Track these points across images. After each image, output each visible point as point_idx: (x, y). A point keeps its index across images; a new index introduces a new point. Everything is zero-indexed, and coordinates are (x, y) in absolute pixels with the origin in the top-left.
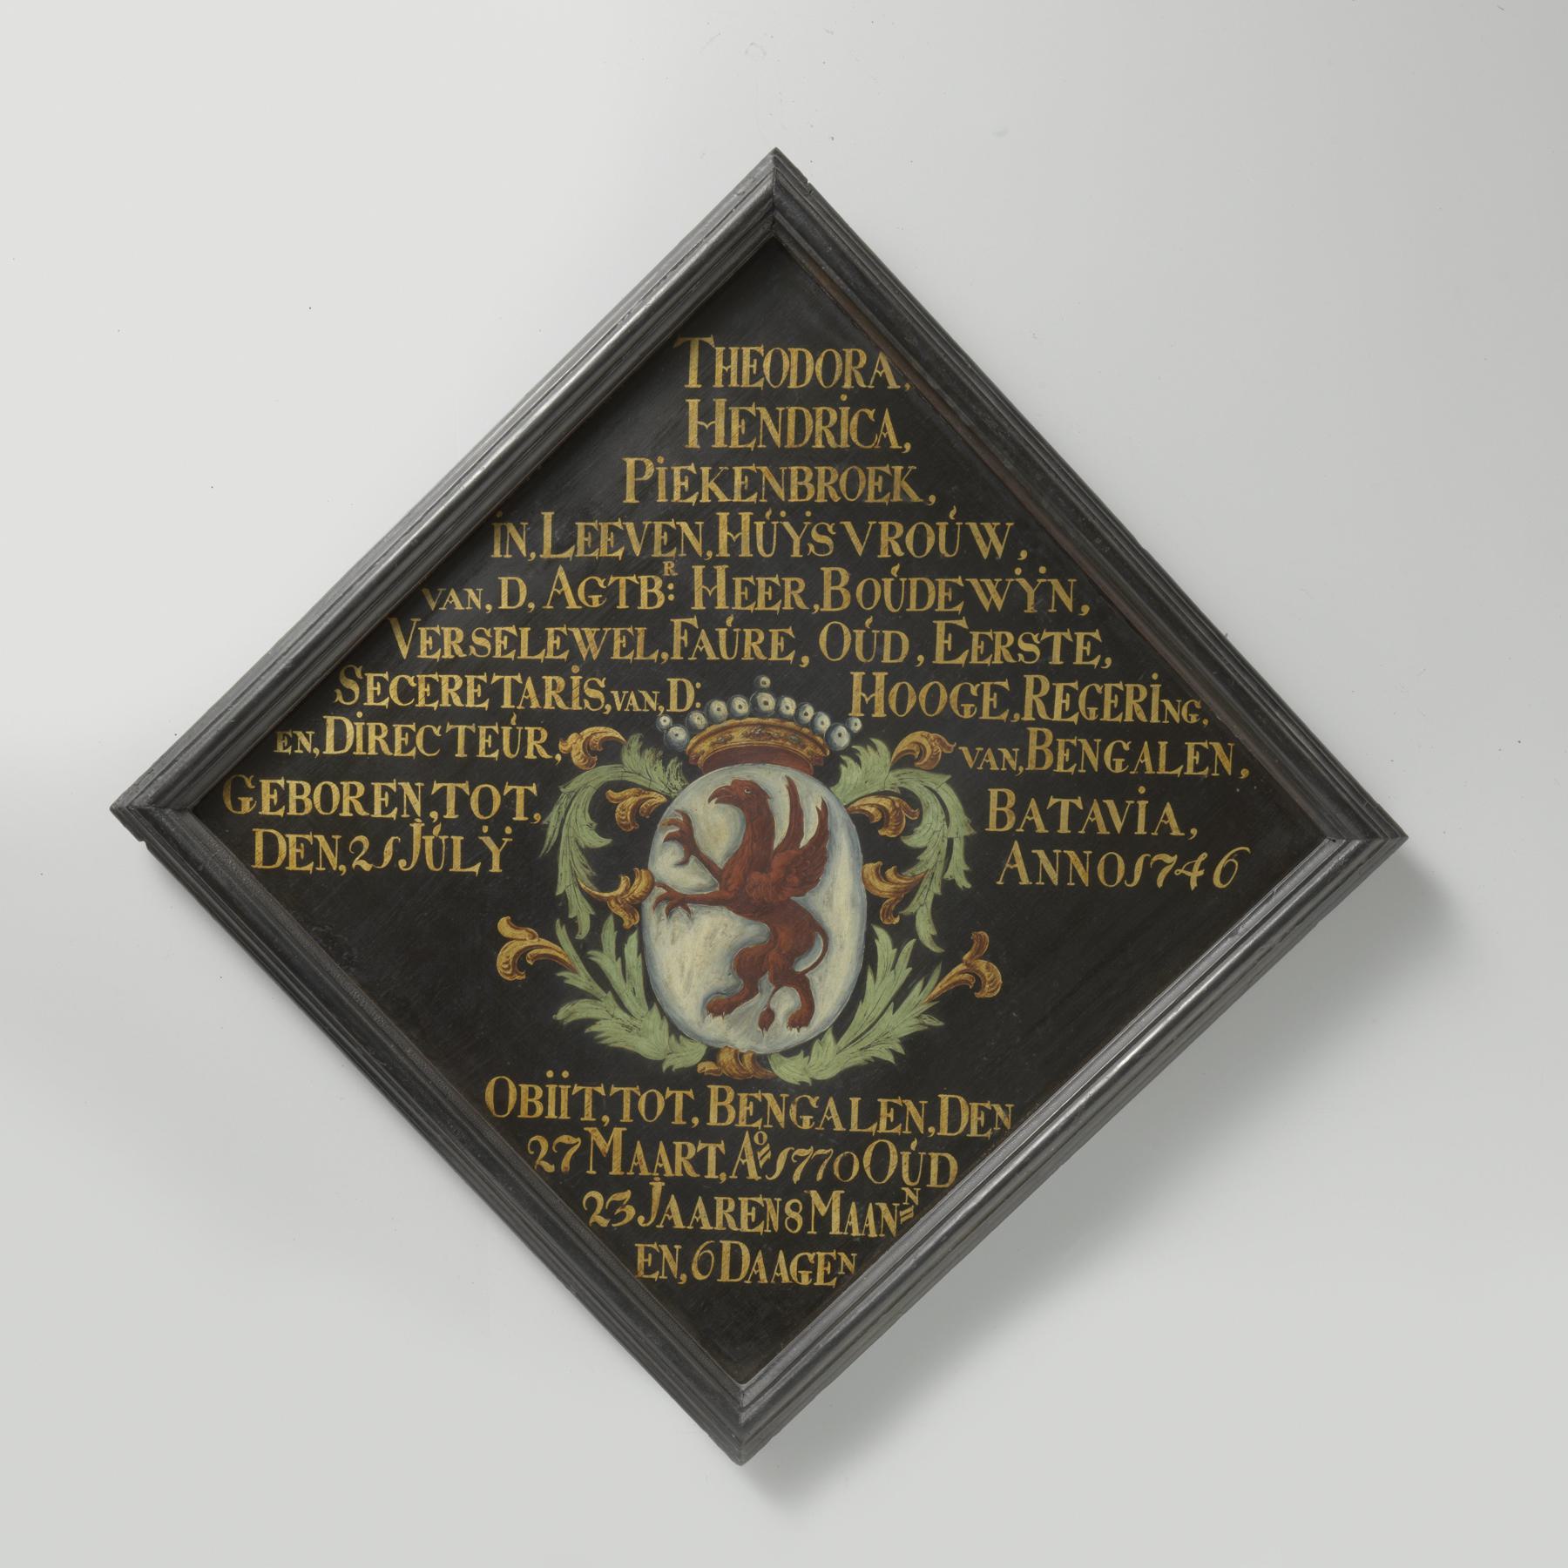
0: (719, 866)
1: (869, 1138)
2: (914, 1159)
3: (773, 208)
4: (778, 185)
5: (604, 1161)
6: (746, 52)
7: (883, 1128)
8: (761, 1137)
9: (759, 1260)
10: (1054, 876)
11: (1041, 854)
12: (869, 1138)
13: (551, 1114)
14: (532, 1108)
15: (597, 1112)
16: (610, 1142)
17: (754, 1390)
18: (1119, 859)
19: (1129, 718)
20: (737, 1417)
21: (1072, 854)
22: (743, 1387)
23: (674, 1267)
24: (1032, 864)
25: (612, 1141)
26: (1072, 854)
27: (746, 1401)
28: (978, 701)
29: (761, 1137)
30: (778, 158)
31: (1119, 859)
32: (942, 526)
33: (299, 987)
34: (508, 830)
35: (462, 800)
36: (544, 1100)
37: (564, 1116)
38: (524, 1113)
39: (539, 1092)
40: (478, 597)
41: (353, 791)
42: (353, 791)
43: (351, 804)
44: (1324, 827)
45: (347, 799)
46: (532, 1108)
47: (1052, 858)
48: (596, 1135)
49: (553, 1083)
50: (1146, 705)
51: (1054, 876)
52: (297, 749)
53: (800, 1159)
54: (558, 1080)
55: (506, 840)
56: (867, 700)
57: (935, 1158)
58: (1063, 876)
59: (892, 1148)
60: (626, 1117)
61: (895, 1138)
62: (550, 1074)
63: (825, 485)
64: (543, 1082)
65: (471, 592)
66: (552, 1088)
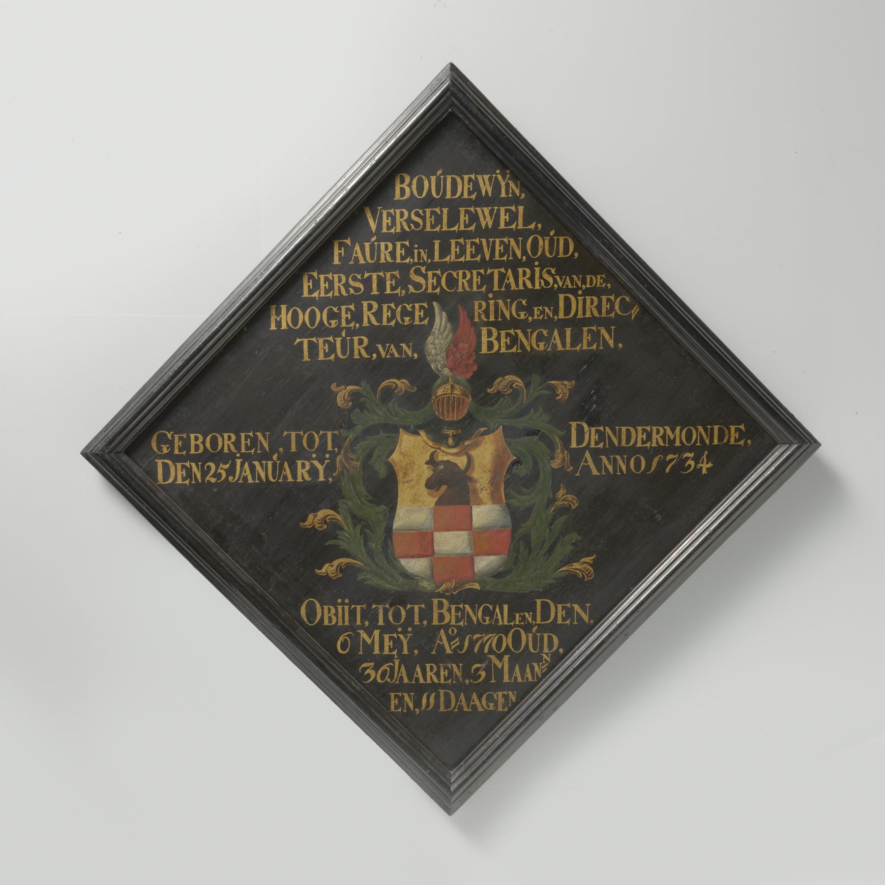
0: (462, 468)
1: (510, 627)
2: (535, 638)
3: (453, 94)
4: (453, 83)
5: (369, 648)
6: (435, 5)
7: (517, 623)
8: (453, 631)
9: (462, 696)
10: (610, 468)
11: (604, 458)
12: (510, 627)
13: (340, 623)
14: (330, 619)
15: (363, 618)
16: (372, 638)
17: (454, 775)
18: (642, 458)
19: (398, 230)
20: (450, 788)
21: (618, 457)
22: (452, 772)
23: (411, 705)
24: (598, 463)
25: (374, 637)
26: (618, 457)
27: (452, 780)
28: (412, 314)
29: (453, 631)
30: (453, 68)
31: (642, 458)
32: (433, 178)
33: (788, 419)
34: (327, 456)
35: (299, 439)
36: (336, 614)
37: (347, 623)
38: (326, 622)
39: (333, 610)
40: (405, 351)
41: (229, 438)
42: (229, 438)
43: (228, 445)
44: (777, 438)
45: (226, 442)
46: (330, 619)
47: (609, 459)
48: (364, 635)
49: (341, 605)
50: (532, 278)
51: (610, 468)
52: (710, 428)
53: (477, 640)
54: (343, 604)
55: (326, 461)
56: (278, 319)
57: (546, 636)
58: (615, 470)
59: (522, 632)
60: (381, 622)
61: (524, 628)
62: (339, 601)
63: (523, 280)
64: (335, 605)
65: (404, 345)
66: (340, 608)
